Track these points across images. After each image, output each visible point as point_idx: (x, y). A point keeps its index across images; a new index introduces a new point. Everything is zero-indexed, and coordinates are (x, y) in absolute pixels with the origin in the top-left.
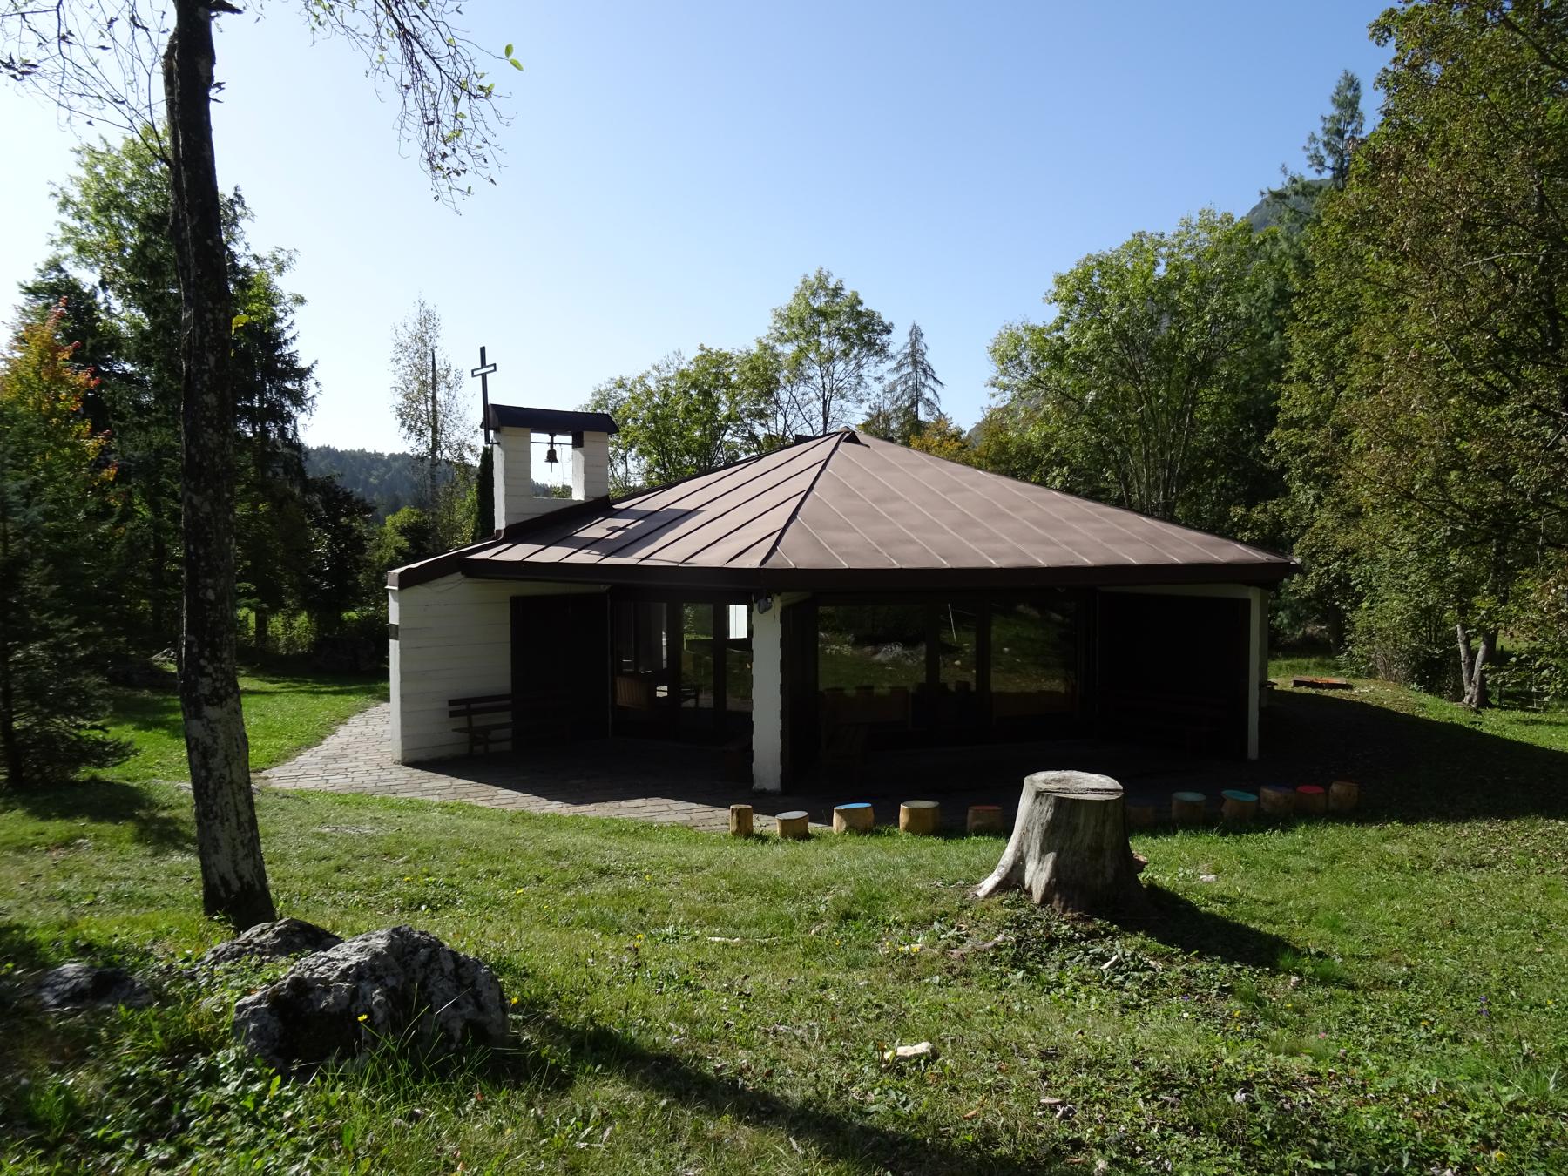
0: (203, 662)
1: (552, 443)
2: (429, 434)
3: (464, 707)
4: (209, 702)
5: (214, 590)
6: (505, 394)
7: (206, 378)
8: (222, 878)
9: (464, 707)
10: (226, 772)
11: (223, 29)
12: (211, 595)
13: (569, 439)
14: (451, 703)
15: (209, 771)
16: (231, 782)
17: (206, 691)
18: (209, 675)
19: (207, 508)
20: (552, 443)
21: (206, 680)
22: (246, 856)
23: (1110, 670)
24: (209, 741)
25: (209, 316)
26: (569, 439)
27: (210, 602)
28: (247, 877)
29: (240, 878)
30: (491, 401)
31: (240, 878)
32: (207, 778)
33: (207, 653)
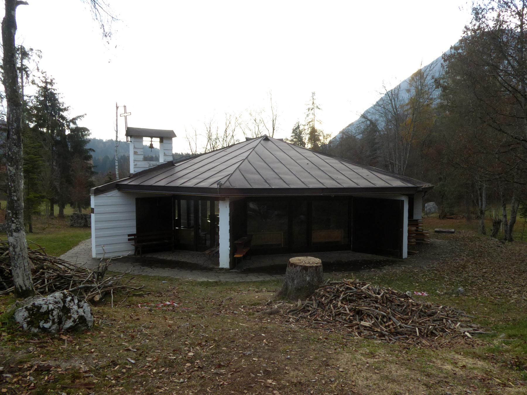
0: (13, 219)
1: (151, 141)
2: (28, 225)
3: (133, 237)
4: (15, 231)
5: (16, 196)
6: (134, 124)
7: (14, 130)
8: (20, 286)
9: (133, 237)
10: (21, 253)
11: (20, 11)
12: (16, 198)
13: (158, 139)
14: (129, 235)
15: (15, 252)
16: (22, 256)
17: (14, 228)
18: (15, 223)
19: (14, 171)
20: (151, 141)
21: (13, 225)
22: (27, 279)
23: (325, 229)
24: (15, 243)
25: (14, 111)
26: (158, 139)
27: (15, 201)
28: (27, 286)
29: (26, 286)
30: (129, 126)
31: (26, 286)
32: (15, 255)
33: (14, 216)
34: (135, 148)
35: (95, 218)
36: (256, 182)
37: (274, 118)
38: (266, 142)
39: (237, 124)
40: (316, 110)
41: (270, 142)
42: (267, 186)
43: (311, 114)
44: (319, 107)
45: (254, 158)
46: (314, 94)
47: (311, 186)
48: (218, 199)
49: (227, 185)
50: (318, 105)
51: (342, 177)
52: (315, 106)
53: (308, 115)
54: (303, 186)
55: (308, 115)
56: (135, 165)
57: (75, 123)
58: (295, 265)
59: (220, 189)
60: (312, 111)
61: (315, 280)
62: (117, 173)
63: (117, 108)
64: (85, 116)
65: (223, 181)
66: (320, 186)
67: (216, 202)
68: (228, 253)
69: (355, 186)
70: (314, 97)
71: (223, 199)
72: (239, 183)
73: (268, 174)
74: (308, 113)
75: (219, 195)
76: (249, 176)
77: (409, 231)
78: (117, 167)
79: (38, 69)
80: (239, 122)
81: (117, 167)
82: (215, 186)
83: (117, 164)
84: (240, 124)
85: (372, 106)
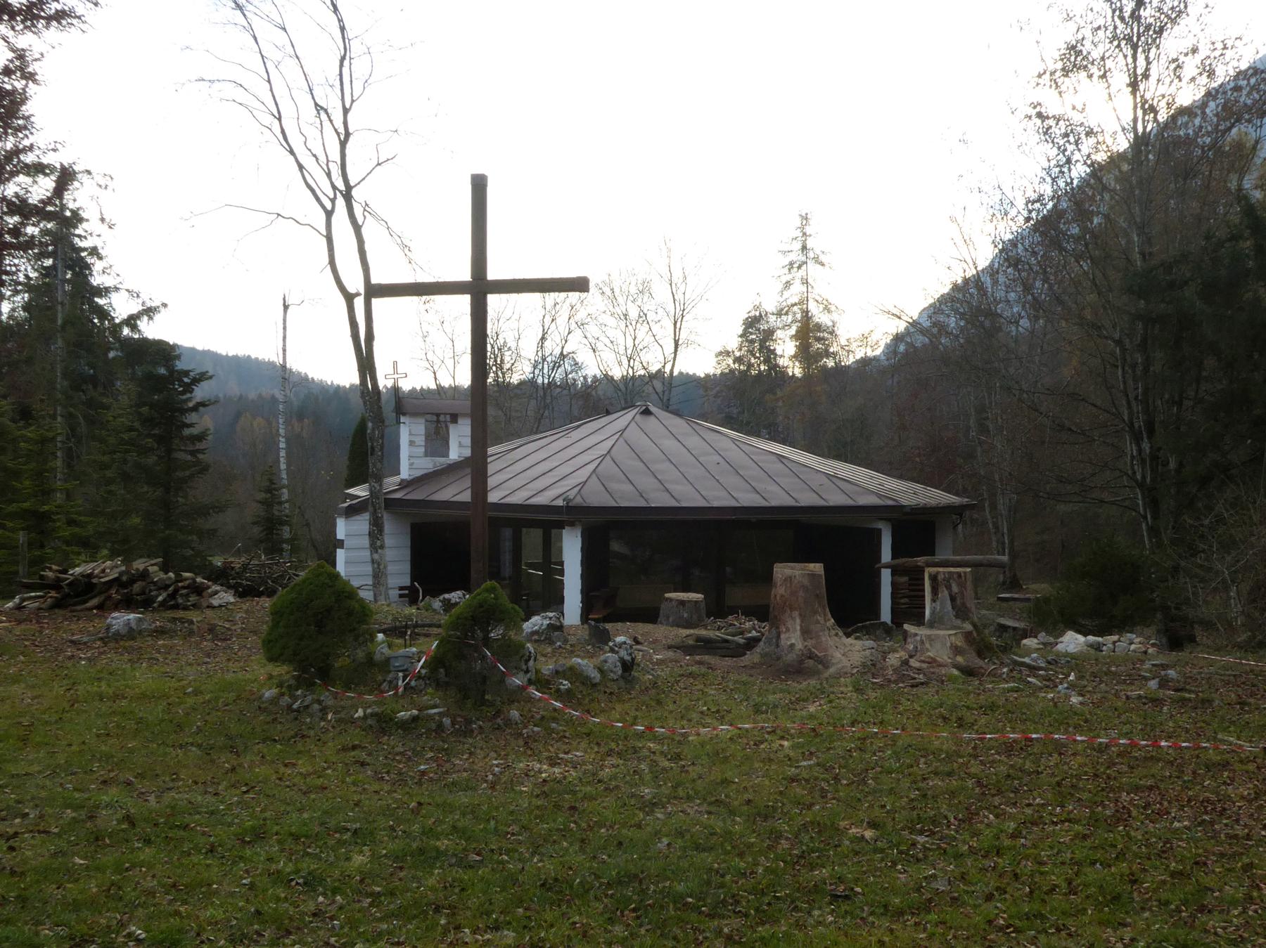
14: (401, 588)
34: (410, 434)
35: (346, 557)
36: (625, 496)
37: (679, 313)
38: (644, 417)
39: (573, 326)
40: (812, 267)
41: (652, 418)
42: (643, 504)
43: (797, 282)
44: (822, 258)
45: (621, 452)
46: (805, 218)
47: (716, 504)
48: (561, 525)
49: (578, 501)
50: (818, 252)
51: (775, 488)
52: (811, 255)
53: (788, 285)
54: (703, 504)
55: (788, 285)
56: (411, 464)
57: (134, 328)
58: (671, 600)
59: (568, 507)
60: (802, 272)
61: (695, 617)
62: (283, 466)
63: (286, 307)
64: (162, 309)
65: (572, 494)
66: (734, 504)
67: (554, 531)
68: (579, 611)
69: (793, 503)
70: (808, 230)
71: (572, 524)
72: (597, 497)
73: (646, 483)
74: (789, 277)
75: (565, 518)
76: (614, 486)
77: (893, 584)
78: (283, 453)
79: (103, 220)
80: (578, 317)
81: (283, 453)
82: (560, 502)
83: (282, 445)
84: (581, 325)
85: (946, 289)
